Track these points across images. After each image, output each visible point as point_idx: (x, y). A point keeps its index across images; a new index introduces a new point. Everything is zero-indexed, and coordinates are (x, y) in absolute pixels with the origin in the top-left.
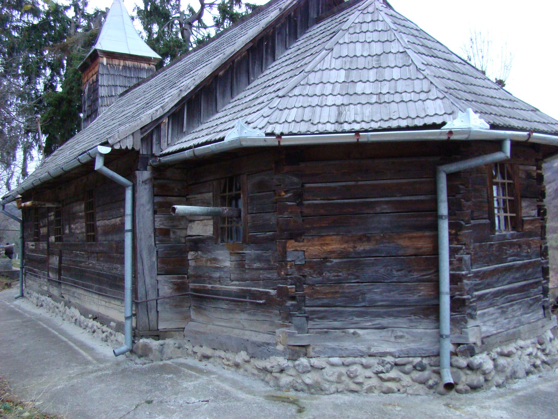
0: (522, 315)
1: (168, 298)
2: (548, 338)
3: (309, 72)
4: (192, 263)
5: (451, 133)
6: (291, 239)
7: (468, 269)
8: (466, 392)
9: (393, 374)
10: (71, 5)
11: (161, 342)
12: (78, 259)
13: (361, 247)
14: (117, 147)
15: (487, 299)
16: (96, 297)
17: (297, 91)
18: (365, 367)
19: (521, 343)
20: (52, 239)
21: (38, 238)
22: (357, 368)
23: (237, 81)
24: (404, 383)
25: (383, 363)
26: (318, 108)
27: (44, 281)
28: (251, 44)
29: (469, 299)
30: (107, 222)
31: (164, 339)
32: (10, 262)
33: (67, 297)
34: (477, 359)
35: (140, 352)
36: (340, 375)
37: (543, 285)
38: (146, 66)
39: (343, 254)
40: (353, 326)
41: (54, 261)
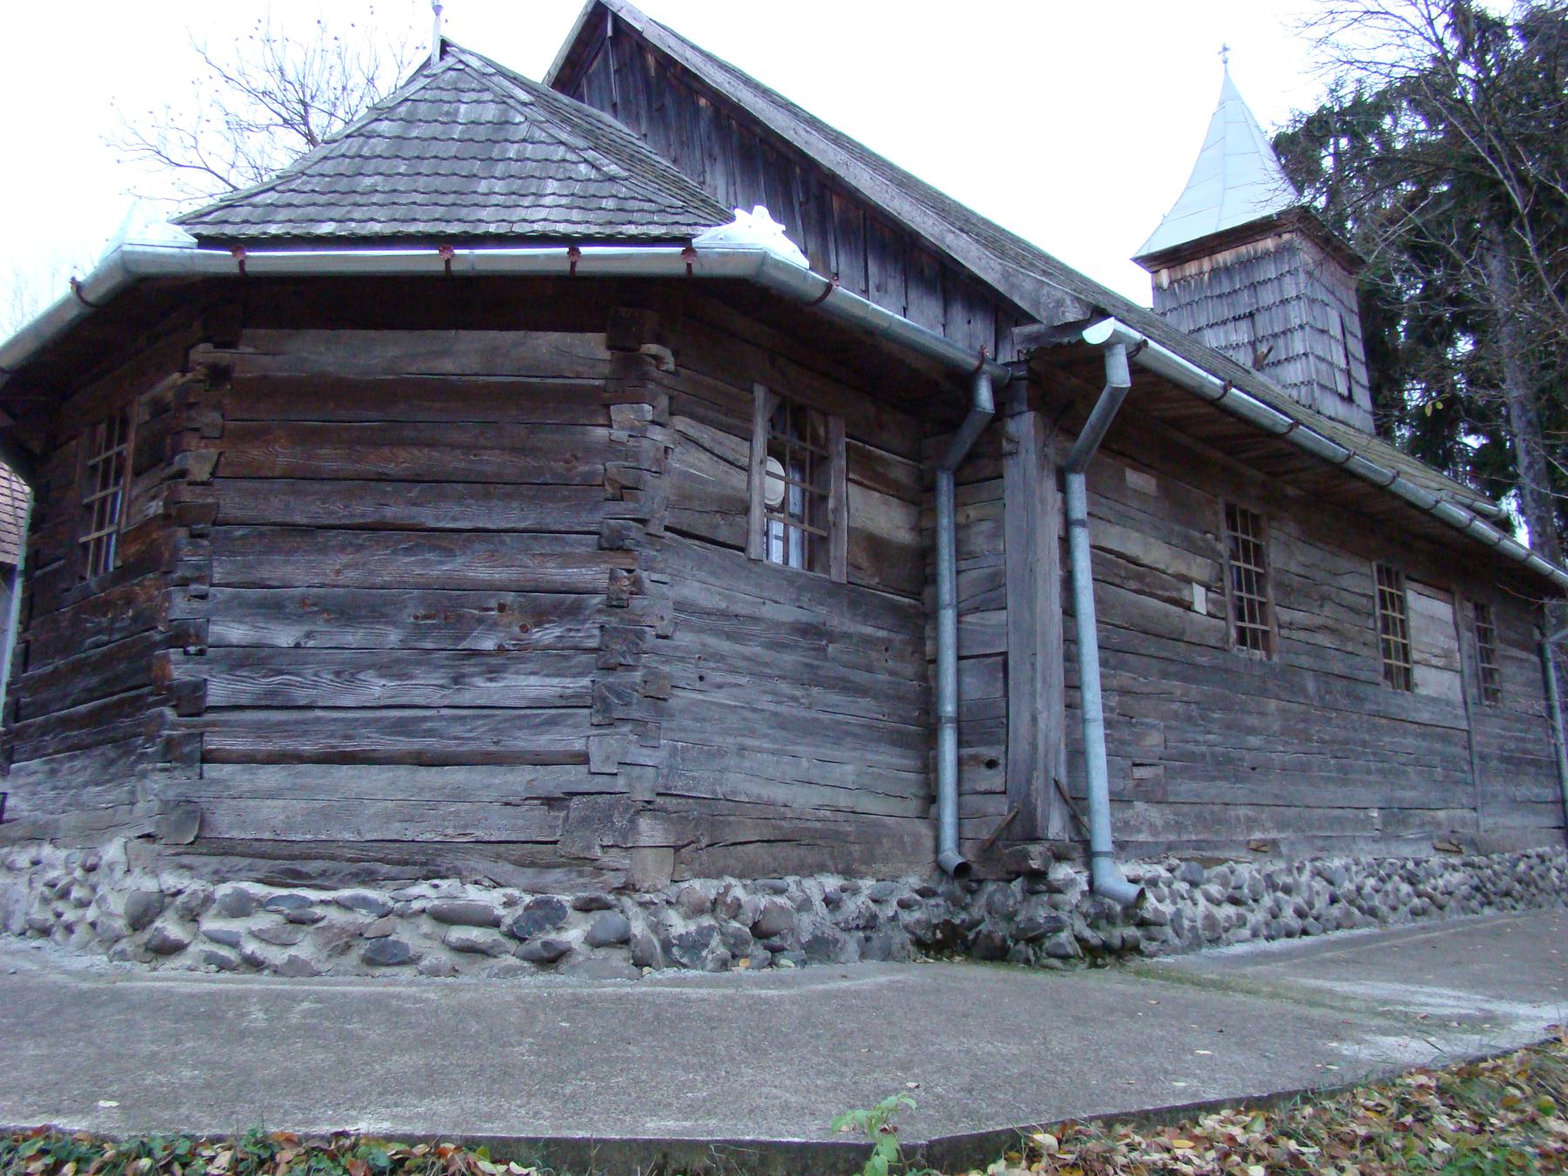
0: (86, 785)
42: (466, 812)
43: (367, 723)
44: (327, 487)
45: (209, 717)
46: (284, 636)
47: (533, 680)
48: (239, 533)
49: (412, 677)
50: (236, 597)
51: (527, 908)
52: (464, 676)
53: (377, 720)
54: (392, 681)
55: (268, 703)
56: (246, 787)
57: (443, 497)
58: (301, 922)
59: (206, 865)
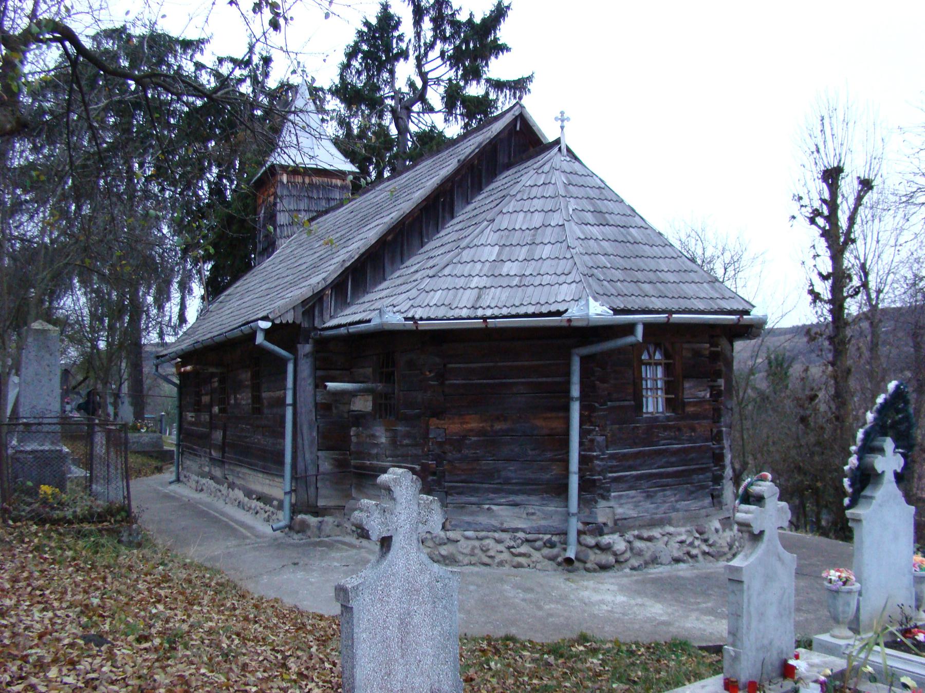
0: (677, 501)
1: (328, 474)
2: (713, 529)
3: (464, 248)
4: (354, 439)
5: (569, 320)
6: (434, 417)
7: (600, 451)
8: (595, 571)
9: (524, 549)
10: (246, 77)
11: (320, 519)
12: (244, 434)
13: (498, 426)
14: (277, 322)
15: (626, 481)
16: (261, 475)
17: (447, 271)
18: (499, 541)
19: (670, 529)
20: (216, 409)
21: (198, 408)
22: (489, 543)
23: (408, 245)
24: (534, 559)
25: (514, 539)
26: (462, 290)
27: (205, 460)
28: (425, 203)
29: (600, 480)
30: (272, 394)
31: (323, 516)
32: (161, 438)
33: (230, 478)
34: (606, 539)
35: (297, 528)
36: (473, 548)
37: (712, 472)
38: (339, 182)
39: (481, 433)
40: (488, 502)
41: (218, 435)
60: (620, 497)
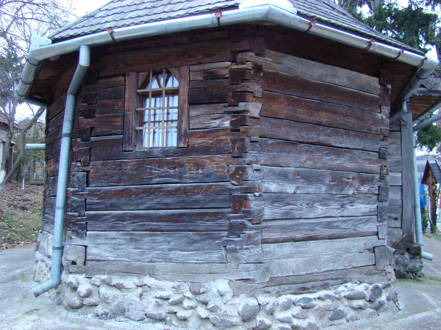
0: (170, 250)
19: (148, 280)
42: (350, 257)
43: (318, 224)
44: (302, 125)
45: (264, 224)
46: (290, 189)
47: (362, 206)
48: (270, 142)
49: (329, 205)
50: (271, 171)
51: (372, 290)
52: (344, 204)
53: (321, 223)
54: (324, 207)
55: (286, 217)
56: (280, 254)
57: (337, 134)
58: (307, 308)
59: (274, 290)
60: (98, 236)
